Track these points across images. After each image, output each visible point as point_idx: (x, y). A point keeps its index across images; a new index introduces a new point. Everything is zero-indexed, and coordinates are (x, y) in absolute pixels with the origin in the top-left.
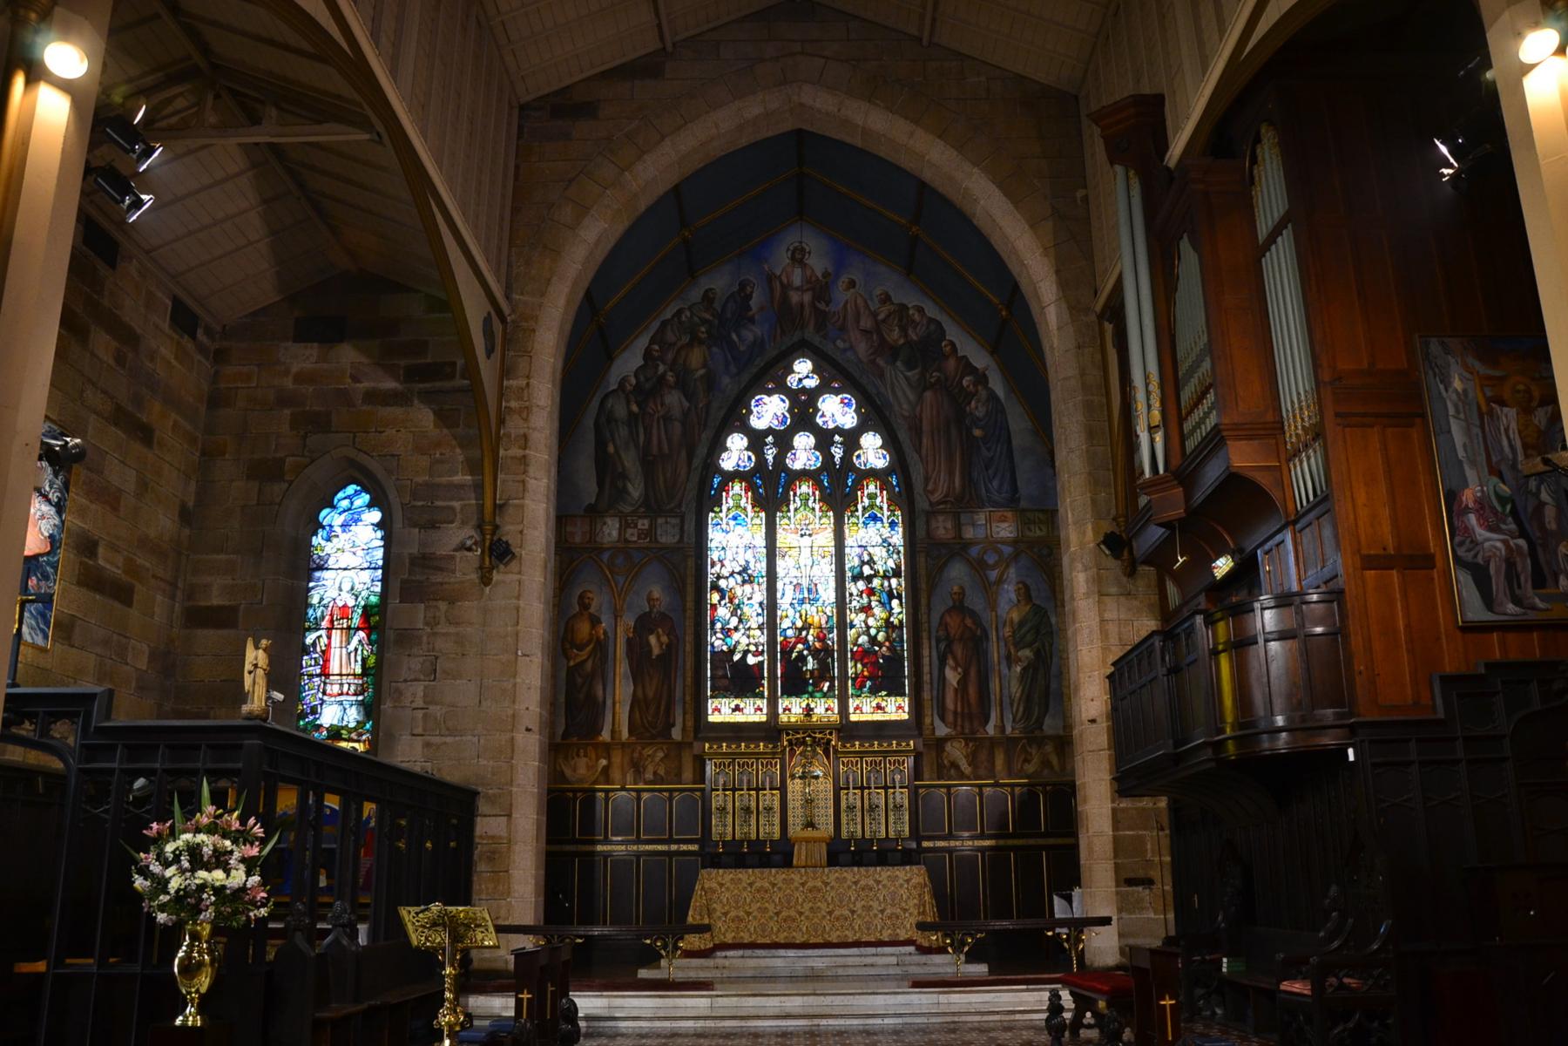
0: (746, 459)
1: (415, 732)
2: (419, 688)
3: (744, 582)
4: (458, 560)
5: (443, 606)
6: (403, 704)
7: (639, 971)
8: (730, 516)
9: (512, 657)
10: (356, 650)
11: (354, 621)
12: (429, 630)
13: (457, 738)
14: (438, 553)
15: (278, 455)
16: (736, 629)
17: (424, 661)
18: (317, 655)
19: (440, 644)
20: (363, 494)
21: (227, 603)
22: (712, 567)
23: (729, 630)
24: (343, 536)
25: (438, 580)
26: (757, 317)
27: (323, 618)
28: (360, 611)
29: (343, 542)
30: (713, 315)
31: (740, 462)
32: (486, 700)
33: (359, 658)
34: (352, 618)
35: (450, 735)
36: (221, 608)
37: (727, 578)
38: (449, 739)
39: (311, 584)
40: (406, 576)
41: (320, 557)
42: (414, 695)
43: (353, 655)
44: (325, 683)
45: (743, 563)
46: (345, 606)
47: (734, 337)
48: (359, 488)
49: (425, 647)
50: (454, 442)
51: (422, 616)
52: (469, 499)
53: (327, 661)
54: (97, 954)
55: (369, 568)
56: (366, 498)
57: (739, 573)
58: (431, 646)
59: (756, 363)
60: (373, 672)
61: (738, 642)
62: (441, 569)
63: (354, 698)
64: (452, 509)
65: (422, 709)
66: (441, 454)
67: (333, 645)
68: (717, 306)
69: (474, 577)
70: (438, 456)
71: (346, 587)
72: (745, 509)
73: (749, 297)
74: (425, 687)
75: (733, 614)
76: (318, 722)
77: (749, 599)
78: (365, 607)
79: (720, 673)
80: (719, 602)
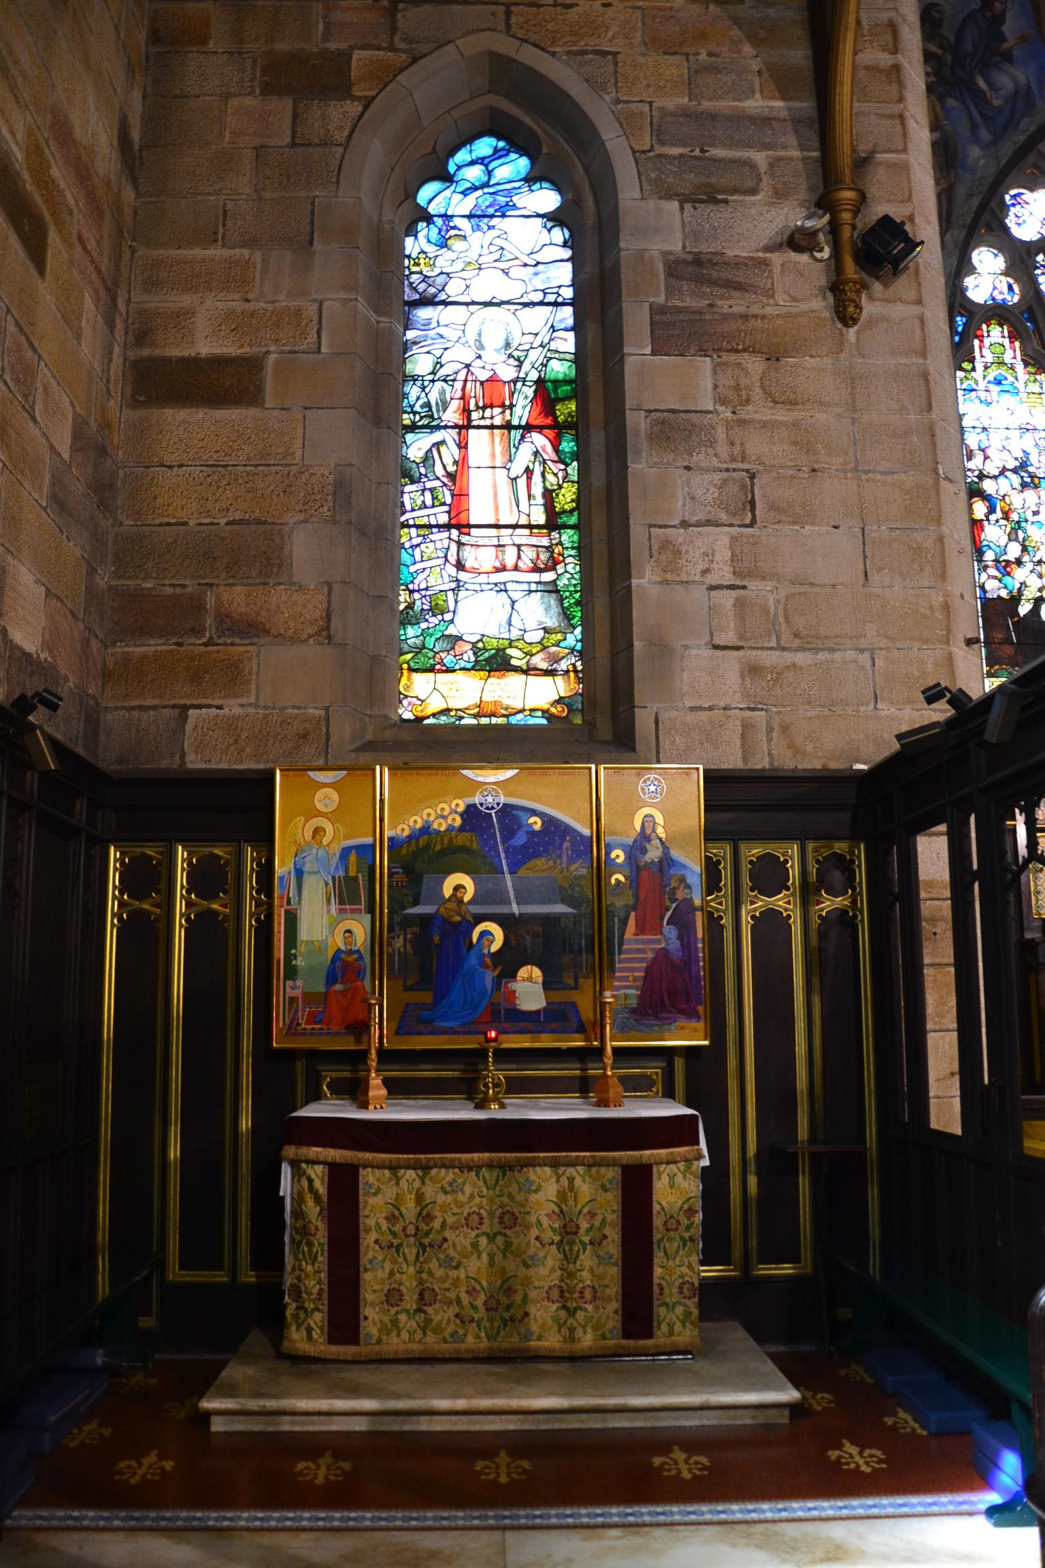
0: (1005, 289)
1: (720, 640)
2: (720, 540)
3: (1024, 486)
4: (777, 269)
5: (754, 365)
6: (684, 578)
7: (286, 1147)
8: (991, 377)
9: (930, 480)
10: (529, 472)
11: (518, 410)
12: (729, 414)
13: (821, 656)
14: (730, 253)
15: (332, 46)
16: (1019, 562)
17: (725, 481)
18: (437, 483)
19: (757, 445)
20: (513, 156)
21: (231, 350)
22: (969, 459)
23: (1008, 563)
24: (476, 239)
25: (737, 309)
26: (1016, 52)
27: (445, 405)
28: (530, 392)
29: (477, 250)
30: (941, 46)
31: (996, 293)
32: (879, 570)
33: (537, 490)
34: (511, 406)
35: (804, 649)
36: (219, 362)
37: (995, 477)
38: (801, 658)
39: (410, 335)
40: (661, 299)
41: (426, 278)
42: (709, 556)
43: (522, 482)
44: (460, 544)
45: (1020, 455)
46: (494, 379)
47: (981, 83)
48: (501, 144)
49: (723, 450)
50: (736, 32)
51: (709, 384)
52: (785, 147)
53: (460, 496)
54: (226, 1268)
55: (541, 303)
56: (522, 164)
57: (1015, 471)
58: (737, 450)
59: (1022, 126)
60: (573, 520)
61: (1023, 584)
62: (740, 287)
63: (535, 577)
64: (752, 165)
65: (732, 587)
66: (710, 54)
67: (473, 460)
68: (948, 32)
69: (821, 305)
70: (703, 56)
71: (494, 341)
72: (1012, 368)
73: (1000, 19)
74: (734, 539)
75: (1012, 536)
76: (451, 630)
77: (1036, 513)
78: (540, 382)
79: (999, 636)
80: (987, 517)
